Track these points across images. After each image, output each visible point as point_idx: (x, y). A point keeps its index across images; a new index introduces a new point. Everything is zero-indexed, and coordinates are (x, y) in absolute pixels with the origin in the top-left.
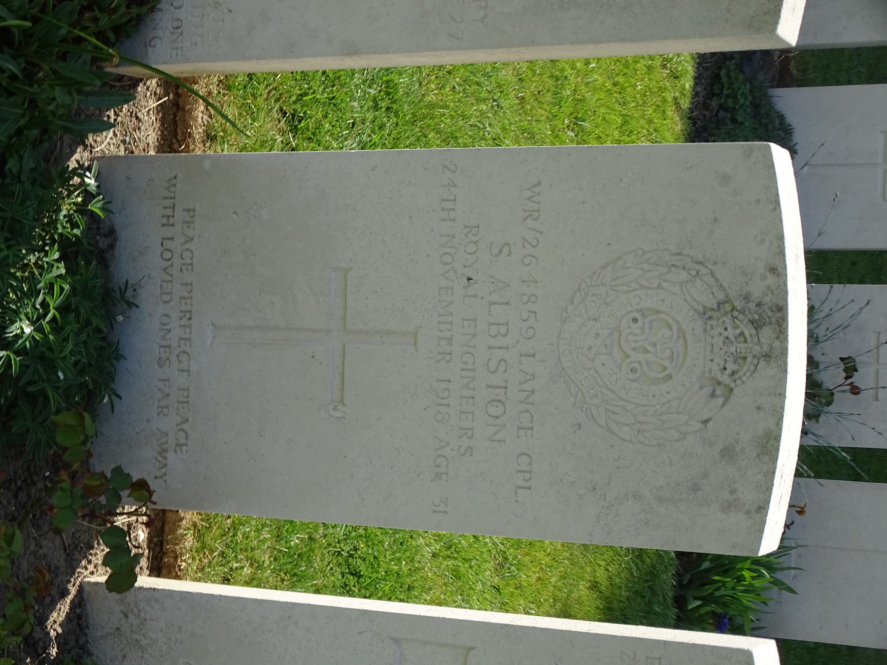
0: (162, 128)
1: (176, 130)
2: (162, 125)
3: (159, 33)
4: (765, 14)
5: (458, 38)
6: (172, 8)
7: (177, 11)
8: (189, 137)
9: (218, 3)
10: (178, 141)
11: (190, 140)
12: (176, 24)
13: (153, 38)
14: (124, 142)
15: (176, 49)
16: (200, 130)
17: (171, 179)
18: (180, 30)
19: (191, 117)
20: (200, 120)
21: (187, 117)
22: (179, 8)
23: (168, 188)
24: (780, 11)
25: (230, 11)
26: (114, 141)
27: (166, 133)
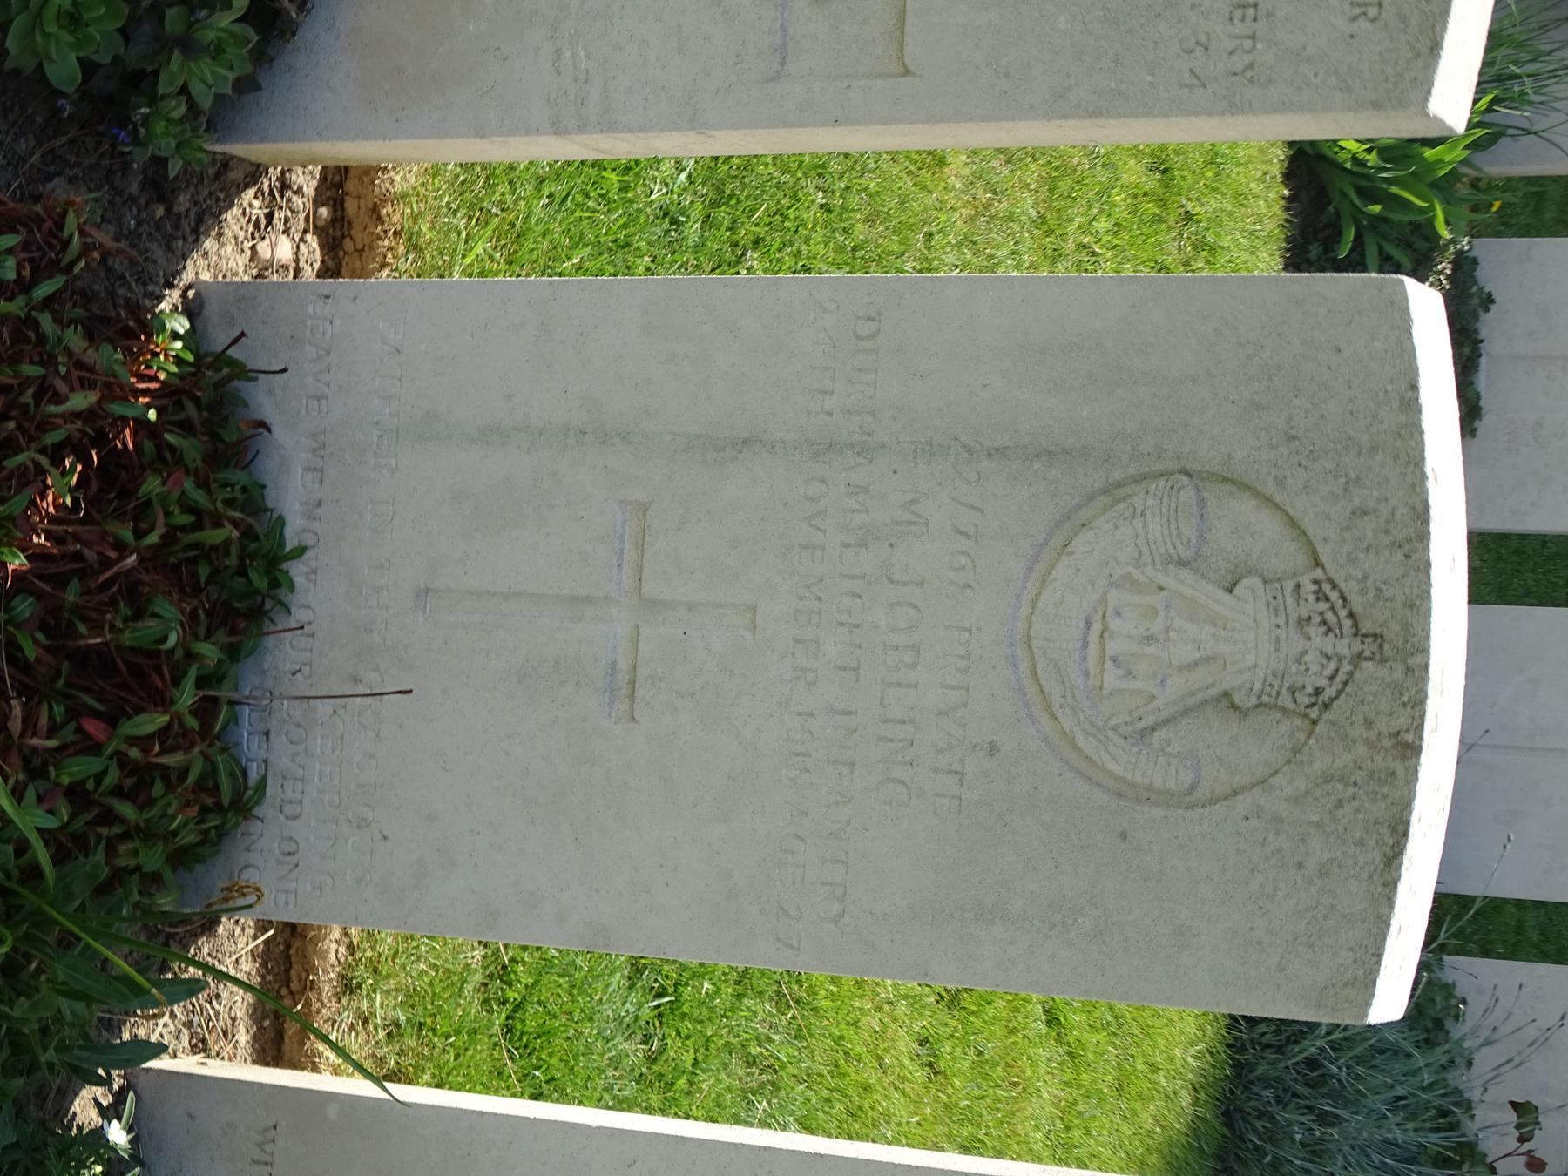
0: (263, 971)
1: (287, 971)
2: (264, 964)
3: (256, 858)
4: (1347, 984)
5: (792, 947)
6: (282, 817)
7: (290, 823)
8: (311, 989)
9: (364, 819)
10: (291, 993)
11: (313, 995)
12: (287, 847)
13: (247, 867)
14: (188, 1024)
15: (286, 892)
16: (332, 975)
17: (266, 1130)
18: (294, 859)
19: (315, 952)
20: (332, 956)
21: (310, 948)
22: (295, 818)
23: (260, 1145)
24: (1374, 982)
25: (385, 838)
26: (172, 1027)
27: (269, 978)
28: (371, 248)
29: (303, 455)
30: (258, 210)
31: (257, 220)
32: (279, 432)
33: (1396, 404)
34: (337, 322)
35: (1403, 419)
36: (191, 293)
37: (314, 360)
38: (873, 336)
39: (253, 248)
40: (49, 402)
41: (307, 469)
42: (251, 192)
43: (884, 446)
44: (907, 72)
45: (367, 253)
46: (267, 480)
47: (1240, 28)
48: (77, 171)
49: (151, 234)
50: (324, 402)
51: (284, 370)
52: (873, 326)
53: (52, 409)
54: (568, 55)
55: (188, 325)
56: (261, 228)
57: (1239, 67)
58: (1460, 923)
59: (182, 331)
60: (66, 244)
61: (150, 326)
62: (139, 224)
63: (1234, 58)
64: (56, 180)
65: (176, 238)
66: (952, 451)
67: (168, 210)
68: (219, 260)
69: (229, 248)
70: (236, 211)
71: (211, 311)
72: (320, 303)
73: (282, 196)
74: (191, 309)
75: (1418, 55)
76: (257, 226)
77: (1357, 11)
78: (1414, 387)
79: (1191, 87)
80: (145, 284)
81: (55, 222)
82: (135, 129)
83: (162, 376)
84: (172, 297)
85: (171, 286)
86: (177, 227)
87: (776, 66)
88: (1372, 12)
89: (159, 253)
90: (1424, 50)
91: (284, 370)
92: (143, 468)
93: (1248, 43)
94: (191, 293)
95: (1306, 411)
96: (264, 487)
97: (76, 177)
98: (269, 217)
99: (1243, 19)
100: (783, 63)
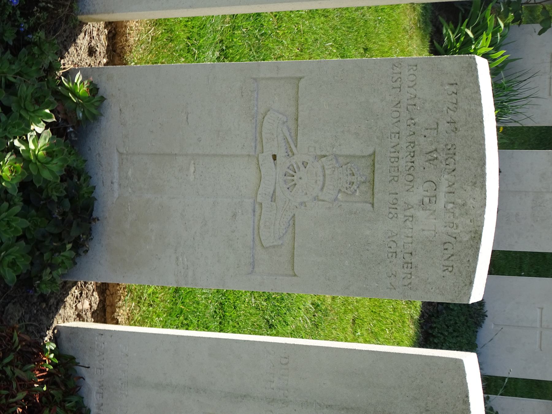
28: (116, 294)
29: (96, 388)
30: (77, 293)
31: (77, 296)
32: (87, 380)
33: (461, 402)
34: (106, 343)
35: (464, 407)
36: (56, 331)
37: (99, 356)
38: (286, 364)
39: (76, 306)
40: (11, 398)
41: (97, 393)
42: (75, 287)
43: (291, 401)
44: (295, 275)
45: (114, 296)
46: (84, 396)
47: (406, 270)
48: (15, 300)
49: (41, 313)
50: (102, 370)
51: (88, 367)
52: (287, 360)
53: (11, 400)
54: (181, 259)
55: (55, 346)
56: (78, 299)
57: (406, 284)
58: (502, 264)
59: (53, 349)
60: (13, 344)
61: (42, 349)
62: (37, 311)
63: (405, 280)
64: (9, 305)
65: (50, 313)
66: (314, 405)
67: (47, 305)
68: (66, 319)
69: (68, 309)
70: (70, 296)
71: (63, 336)
72: (100, 336)
73: (85, 286)
74: (55, 339)
75: (466, 285)
76: (77, 298)
77: (446, 268)
78: (467, 397)
79: (391, 289)
80: (40, 333)
81: (10, 337)
82: (35, 289)
83: (47, 370)
84: (50, 333)
85: (48, 329)
86: (50, 309)
87: (251, 269)
88: (450, 269)
89: (44, 318)
90: (468, 284)
91: (88, 367)
92: (43, 407)
93: (409, 276)
94: (56, 331)
95: (432, 401)
96: (83, 398)
97: (16, 302)
98: (81, 294)
99: (407, 268)
100: (253, 268)
